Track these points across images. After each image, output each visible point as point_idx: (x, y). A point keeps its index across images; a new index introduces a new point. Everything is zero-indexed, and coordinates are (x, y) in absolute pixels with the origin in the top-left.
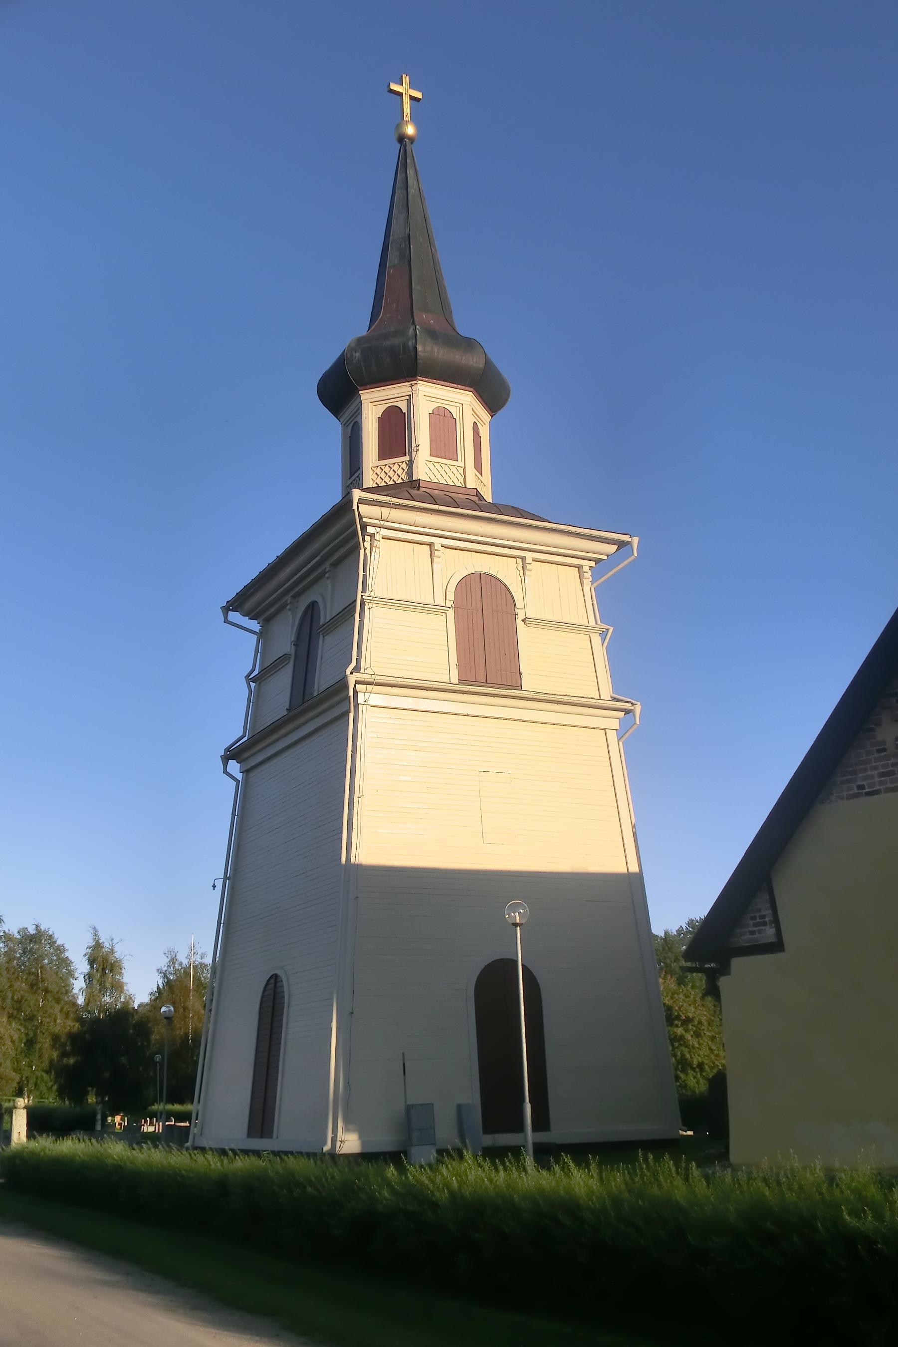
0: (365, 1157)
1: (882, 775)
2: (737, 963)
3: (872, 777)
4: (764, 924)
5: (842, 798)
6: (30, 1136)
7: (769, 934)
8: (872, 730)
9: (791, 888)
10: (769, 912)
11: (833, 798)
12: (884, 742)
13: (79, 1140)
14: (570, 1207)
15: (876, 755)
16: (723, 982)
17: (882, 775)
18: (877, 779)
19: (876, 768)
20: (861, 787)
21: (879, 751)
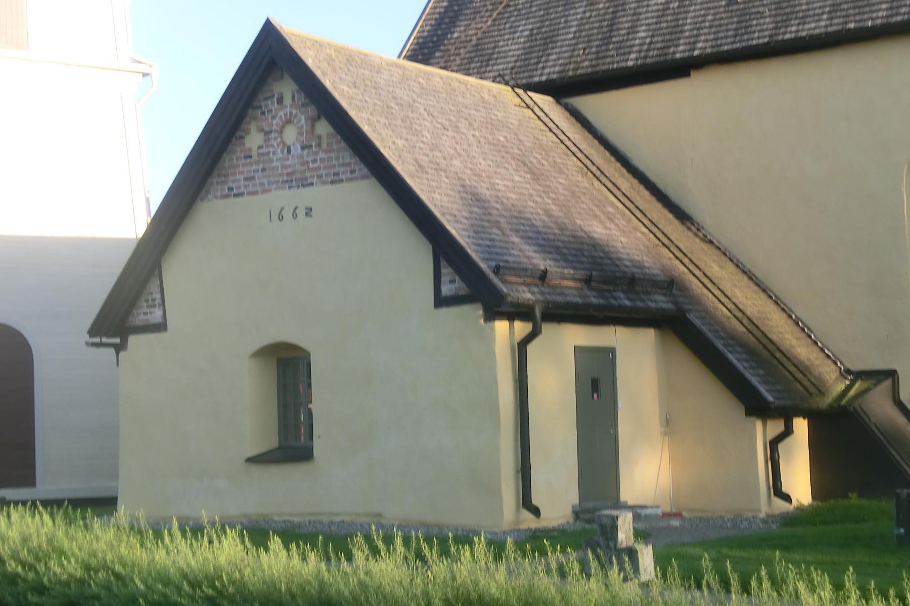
0: (434, 52)
1: (246, 179)
2: (133, 340)
3: (239, 180)
4: (154, 306)
5: (216, 197)
6: (614, 519)
7: (156, 316)
8: (242, 138)
9: (179, 271)
10: (158, 296)
11: (210, 197)
12: (250, 150)
13: (726, 585)
14: (737, 49)
15: (243, 161)
16: (122, 354)
17: (246, 179)
18: (242, 183)
19: (242, 172)
20: (231, 189)
21: (246, 157)
